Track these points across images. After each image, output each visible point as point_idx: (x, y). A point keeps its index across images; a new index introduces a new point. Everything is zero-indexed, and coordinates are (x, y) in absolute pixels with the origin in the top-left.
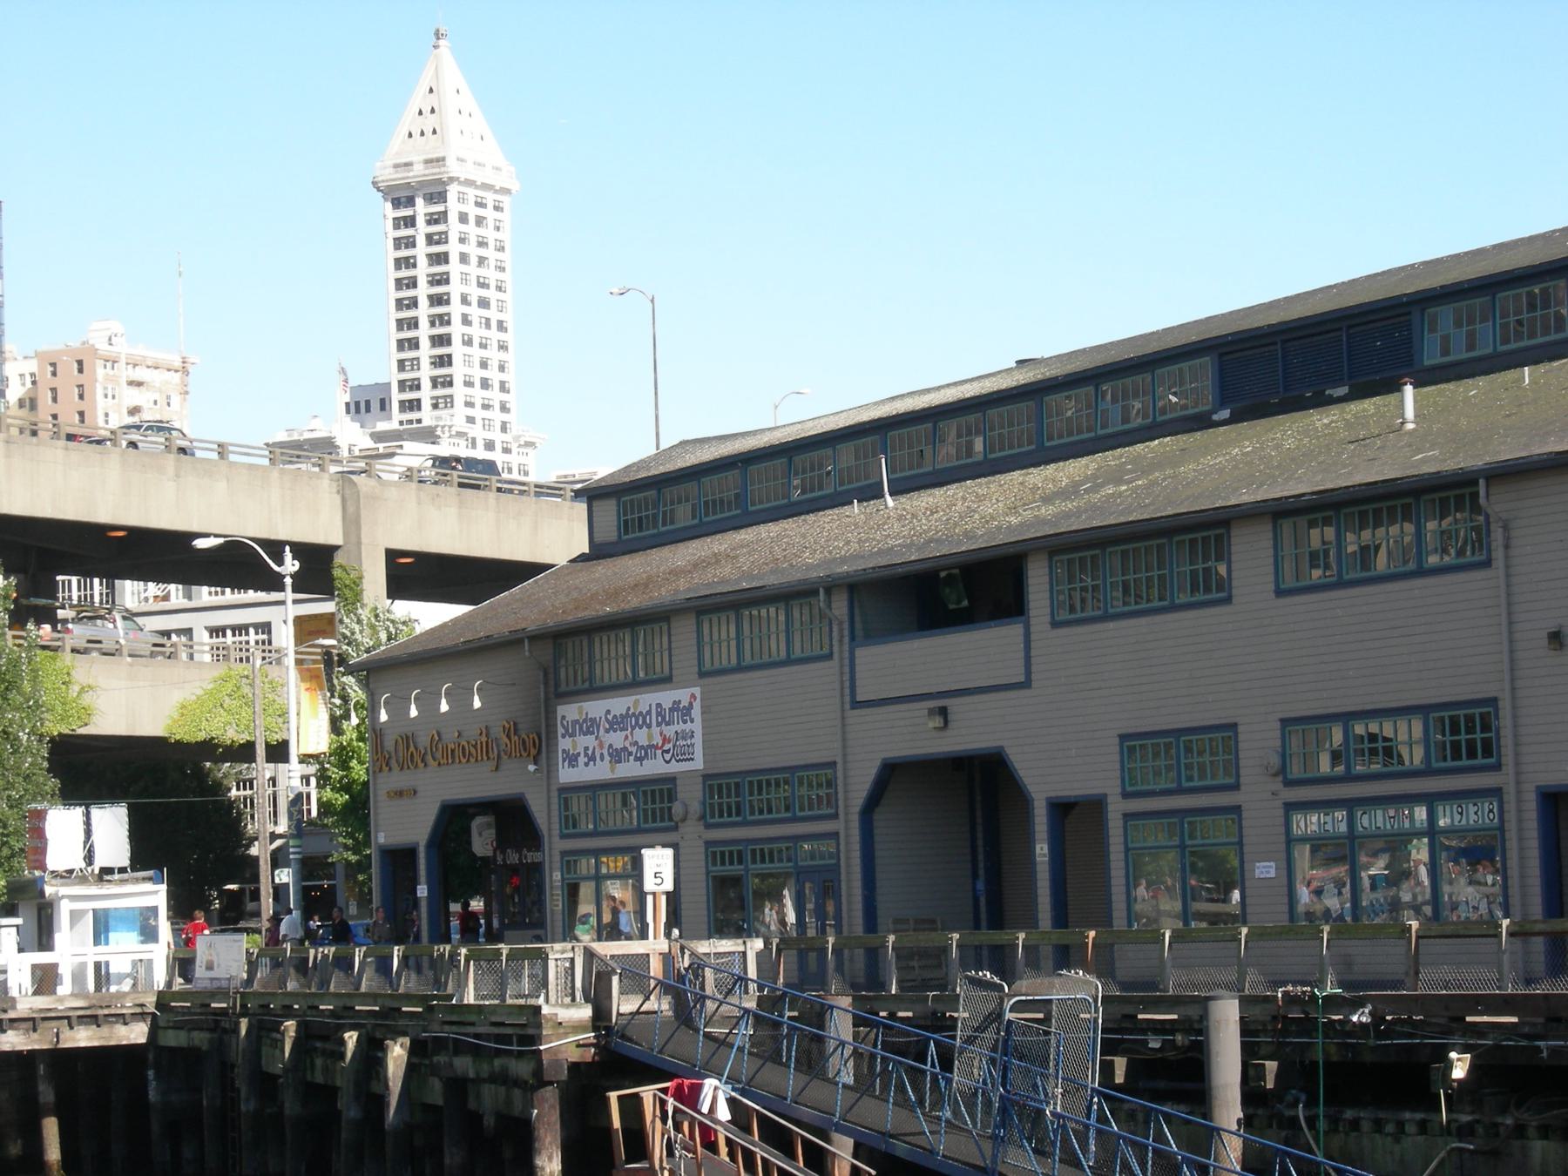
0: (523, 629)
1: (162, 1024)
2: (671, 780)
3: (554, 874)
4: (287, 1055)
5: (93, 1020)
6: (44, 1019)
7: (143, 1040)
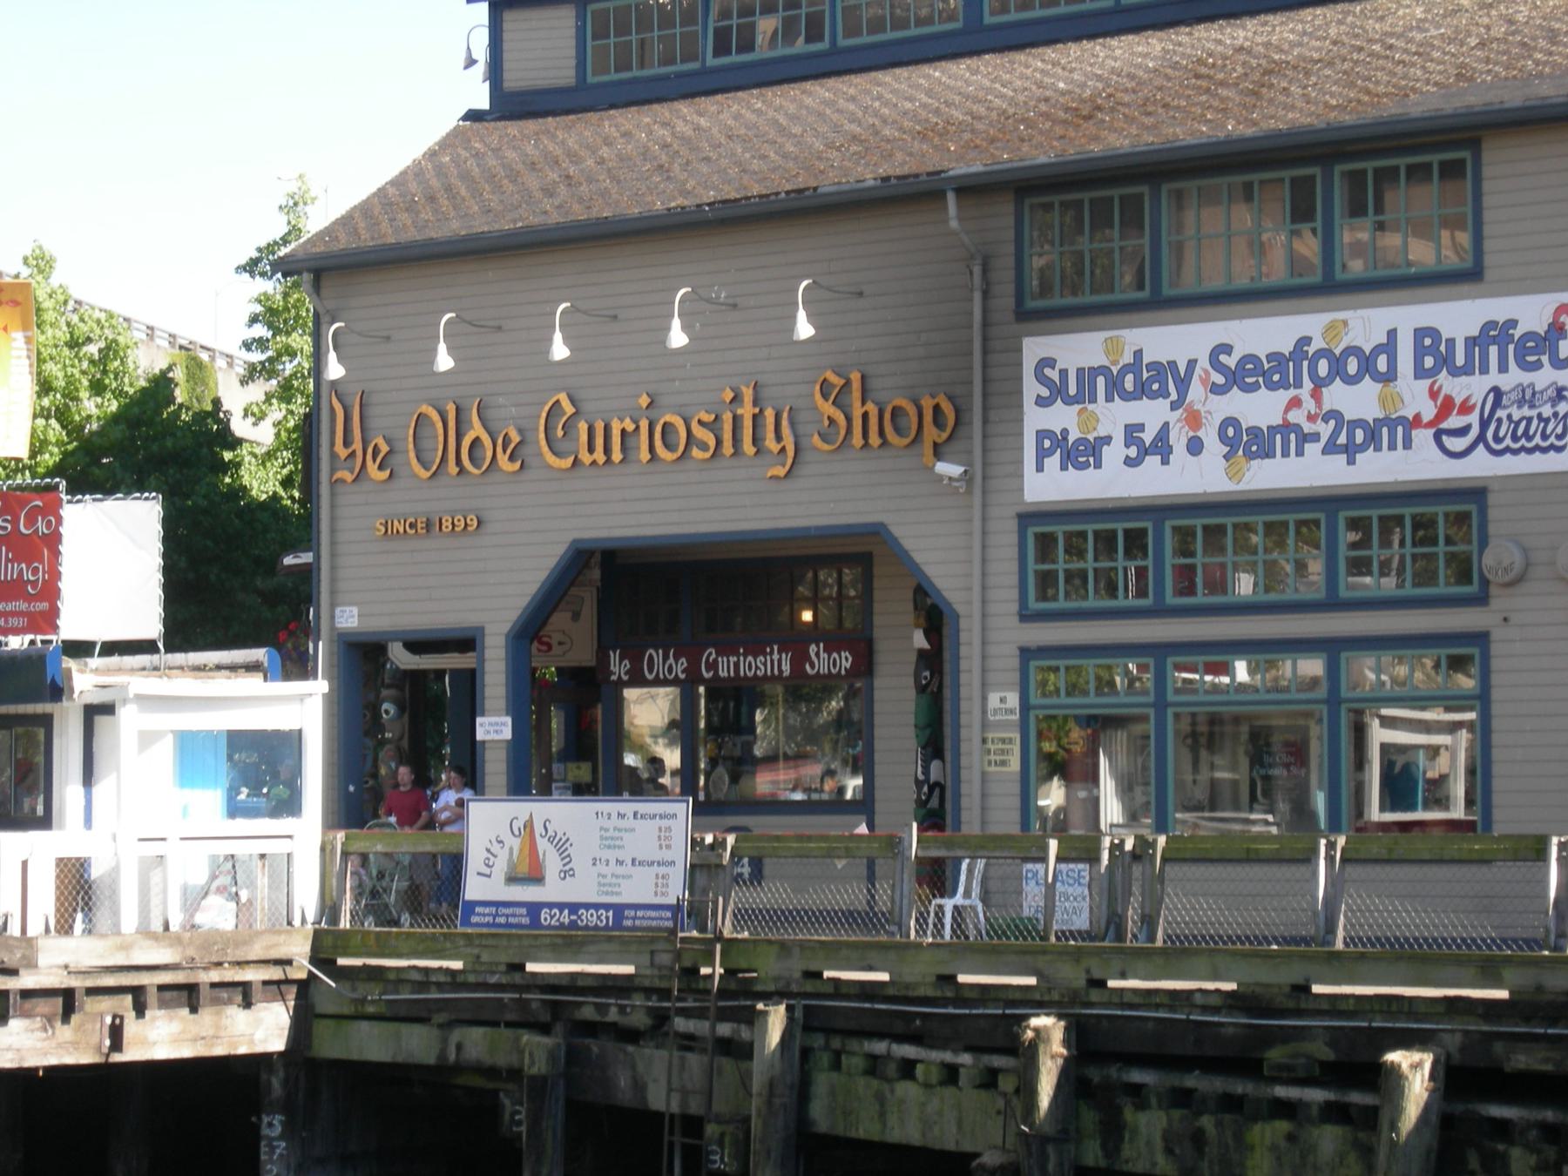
0: (815, 189)
1: (324, 1005)
2: (1475, 494)
3: (994, 700)
4: (1045, 1097)
5: (188, 996)
6: (93, 991)
7: (277, 1044)
